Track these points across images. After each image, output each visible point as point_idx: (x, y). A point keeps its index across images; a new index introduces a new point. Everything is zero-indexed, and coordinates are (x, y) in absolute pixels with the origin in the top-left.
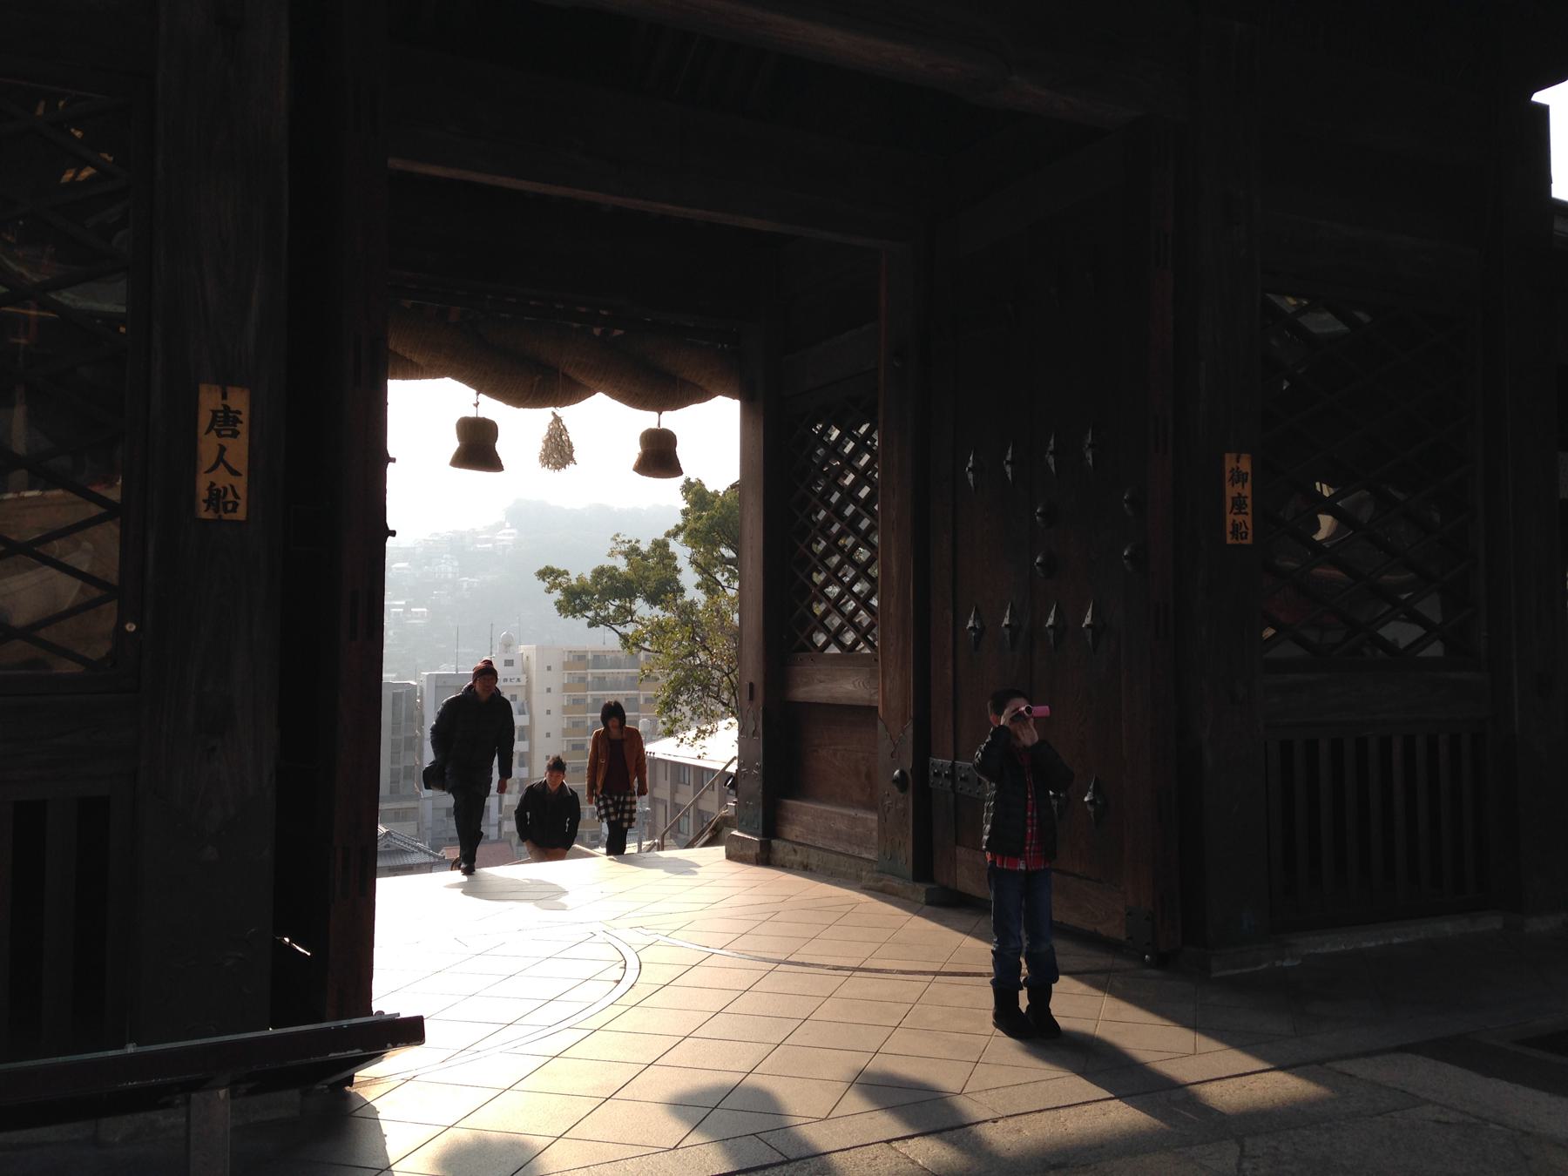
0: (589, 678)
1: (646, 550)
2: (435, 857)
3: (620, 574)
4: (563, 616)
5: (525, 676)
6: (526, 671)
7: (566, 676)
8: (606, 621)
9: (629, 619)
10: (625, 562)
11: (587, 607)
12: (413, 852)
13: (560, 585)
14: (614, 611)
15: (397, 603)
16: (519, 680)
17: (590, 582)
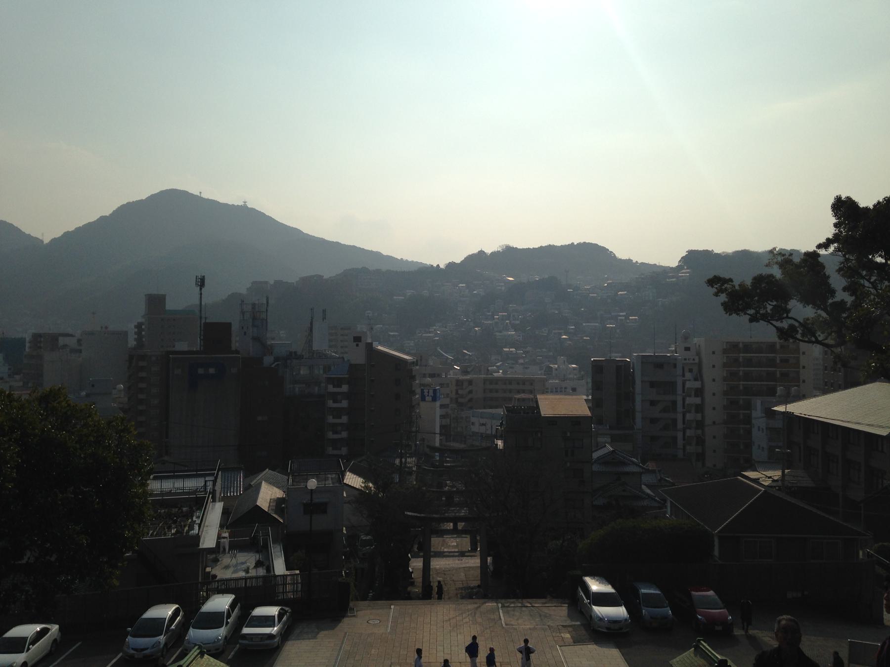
0: (741, 360)
1: (798, 261)
2: (643, 468)
3: (776, 280)
4: (728, 314)
5: (697, 357)
6: (698, 354)
7: (725, 358)
8: (766, 318)
9: (785, 315)
10: (780, 271)
11: (748, 306)
12: (629, 464)
13: (726, 289)
14: (771, 310)
15: (621, 314)
16: (694, 360)
17: (750, 288)
